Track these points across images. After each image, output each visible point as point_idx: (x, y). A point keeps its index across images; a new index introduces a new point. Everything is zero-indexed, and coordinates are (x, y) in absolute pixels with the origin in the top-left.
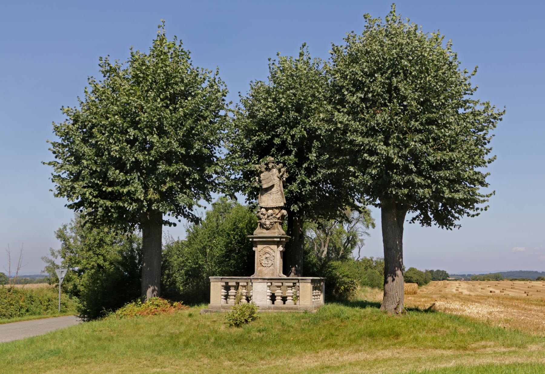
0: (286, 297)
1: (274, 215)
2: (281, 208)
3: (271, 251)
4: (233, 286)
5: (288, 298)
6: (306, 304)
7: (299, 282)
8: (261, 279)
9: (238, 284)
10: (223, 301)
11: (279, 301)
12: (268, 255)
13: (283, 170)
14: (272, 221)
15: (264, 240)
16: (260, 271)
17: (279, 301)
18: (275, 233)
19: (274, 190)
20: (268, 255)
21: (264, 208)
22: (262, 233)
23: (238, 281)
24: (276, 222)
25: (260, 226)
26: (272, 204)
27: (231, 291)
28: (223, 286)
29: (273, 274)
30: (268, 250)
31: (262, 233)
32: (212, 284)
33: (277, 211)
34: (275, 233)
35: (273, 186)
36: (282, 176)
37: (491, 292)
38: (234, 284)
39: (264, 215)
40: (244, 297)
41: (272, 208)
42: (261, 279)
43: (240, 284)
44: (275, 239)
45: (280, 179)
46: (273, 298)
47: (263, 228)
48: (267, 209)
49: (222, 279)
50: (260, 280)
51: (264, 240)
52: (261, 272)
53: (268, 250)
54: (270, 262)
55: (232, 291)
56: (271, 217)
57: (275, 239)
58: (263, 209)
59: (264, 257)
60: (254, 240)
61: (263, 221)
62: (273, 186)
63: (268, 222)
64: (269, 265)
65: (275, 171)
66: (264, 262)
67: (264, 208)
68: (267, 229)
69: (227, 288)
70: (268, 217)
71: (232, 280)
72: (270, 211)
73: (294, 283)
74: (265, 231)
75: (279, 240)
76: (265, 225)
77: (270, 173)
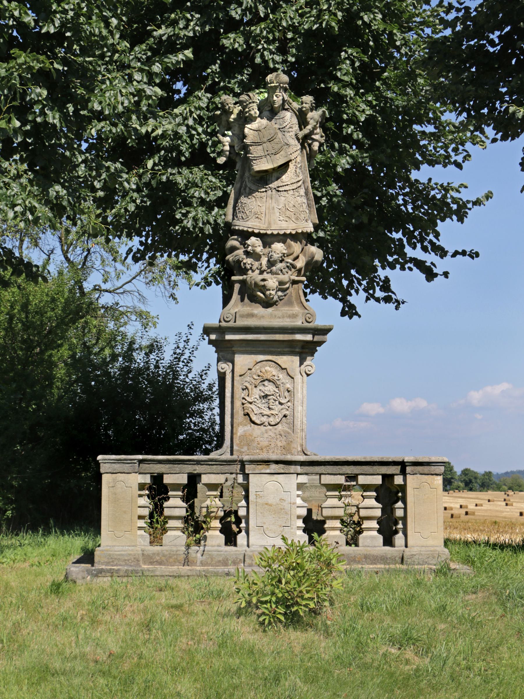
0: (324, 522)
1: (289, 260)
2: (307, 238)
3: (282, 376)
4: (176, 487)
5: (329, 524)
6: (430, 542)
7: (403, 472)
8: (277, 462)
9: (194, 479)
10: (142, 538)
11: (334, 533)
12: (269, 388)
13: (314, 116)
14: (285, 278)
15: (262, 337)
16: (243, 437)
17: (334, 533)
18: (294, 316)
19: (287, 178)
20: (269, 388)
21: (258, 235)
22: (252, 315)
23: (198, 469)
24: (294, 282)
25: (241, 293)
26: (284, 225)
27: (171, 502)
28: (142, 487)
29: (287, 449)
30: (271, 371)
31: (252, 315)
32: (105, 478)
33: (297, 247)
34: (294, 316)
35: (284, 167)
36: (307, 137)
37: (476, 505)
38: (183, 479)
39: (257, 257)
40: (216, 524)
41: (283, 238)
42: (277, 462)
43: (205, 479)
44: (299, 337)
45: (303, 147)
46: (313, 526)
47: (254, 299)
48: (267, 239)
49: (141, 461)
50: (274, 468)
51: (262, 337)
52: (248, 441)
53: (271, 371)
54: (277, 408)
55: (175, 505)
56: (280, 265)
57: (299, 337)
58: (253, 239)
59: (256, 393)
60: (228, 337)
61: (254, 276)
62: (285, 167)
63: (272, 282)
64: (272, 420)
65: (289, 118)
66: (258, 409)
67: (258, 235)
68: (268, 304)
69: (158, 490)
70: (271, 263)
71: (177, 467)
72: (278, 247)
73: (385, 477)
74: (258, 310)
75: (309, 337)
76: (264, 289)
77: (274, 124)
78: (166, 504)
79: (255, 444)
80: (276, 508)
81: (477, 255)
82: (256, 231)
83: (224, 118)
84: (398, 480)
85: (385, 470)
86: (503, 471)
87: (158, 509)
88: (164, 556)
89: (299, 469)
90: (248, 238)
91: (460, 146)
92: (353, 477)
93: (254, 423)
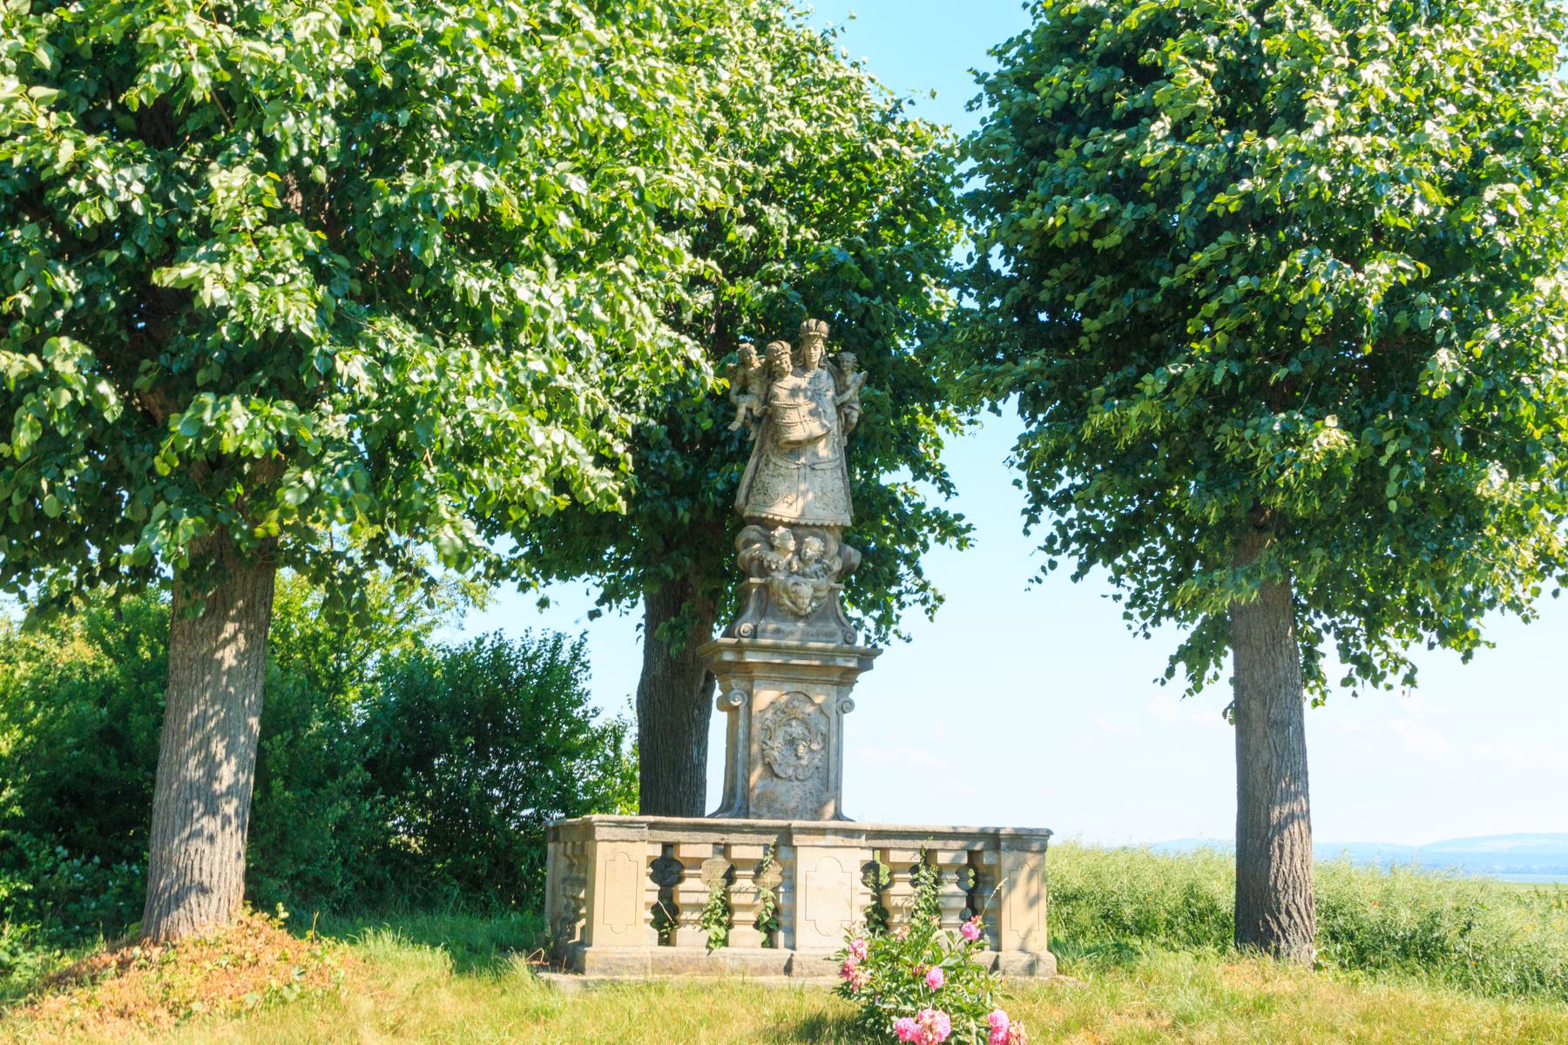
26: (821, 513)
49: (652, 826)
50: (831, 839)
71: (699, 836)
78: (681, 887)
79: (778, 806)
80: (830, 889)
81: (1494, 646)
82: (786, 520)
83: (741, 372)
84: (987, 859)
85: (929, 844)
86: (1118, 843)
87: (667, 894)
88: (681, 961)
89: (838, 840)
90: (775, 528)
91: (278, 204)
92: (884, 851)
93: (777, 776)
